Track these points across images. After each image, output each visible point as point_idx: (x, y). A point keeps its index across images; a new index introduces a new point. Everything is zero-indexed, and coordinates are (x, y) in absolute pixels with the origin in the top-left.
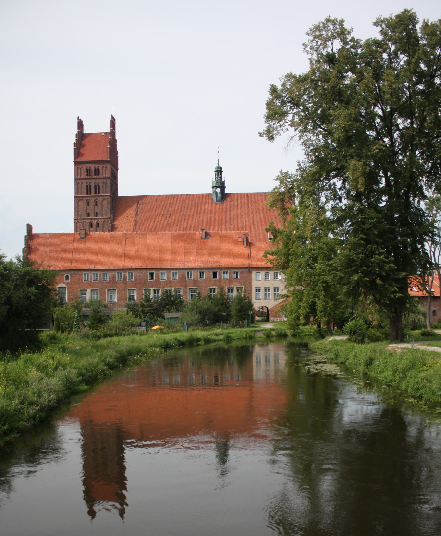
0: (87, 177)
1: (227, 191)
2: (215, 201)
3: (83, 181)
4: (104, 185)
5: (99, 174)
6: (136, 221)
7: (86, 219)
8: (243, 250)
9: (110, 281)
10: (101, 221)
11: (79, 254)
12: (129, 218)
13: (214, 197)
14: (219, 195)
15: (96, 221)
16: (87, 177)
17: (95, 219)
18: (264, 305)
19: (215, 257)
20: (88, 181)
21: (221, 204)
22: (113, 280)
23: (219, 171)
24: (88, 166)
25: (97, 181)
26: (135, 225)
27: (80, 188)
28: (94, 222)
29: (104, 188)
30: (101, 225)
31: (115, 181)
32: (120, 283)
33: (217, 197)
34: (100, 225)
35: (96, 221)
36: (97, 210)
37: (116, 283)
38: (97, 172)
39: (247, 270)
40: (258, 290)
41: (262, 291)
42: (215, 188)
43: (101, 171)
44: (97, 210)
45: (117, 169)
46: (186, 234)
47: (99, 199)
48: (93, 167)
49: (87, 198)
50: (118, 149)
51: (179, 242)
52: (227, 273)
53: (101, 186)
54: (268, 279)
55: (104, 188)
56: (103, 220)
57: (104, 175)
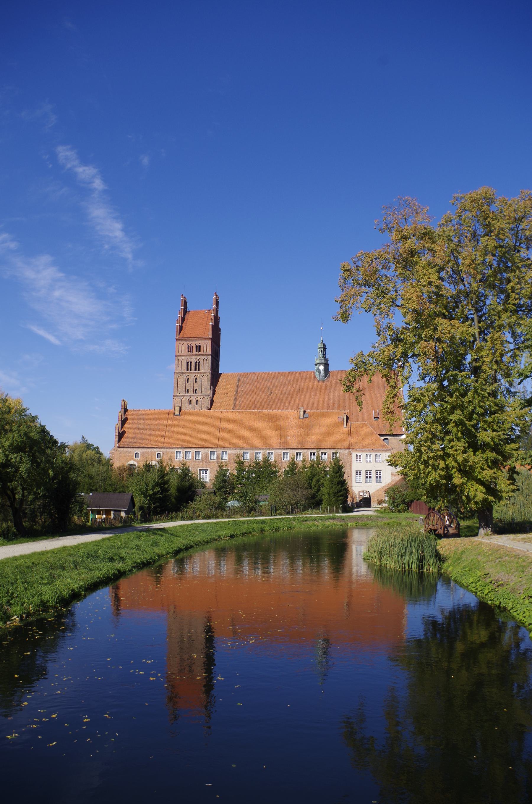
0: (188, 353)
1: (330, 368)
2: (318, 378)
3: (184, 357)
4: (205, 362)
5: (200, 351)
6: (236, 398)
7: (185, 396)
8: (342, 431)
9: (202, 460)
10: (199, 398)
11: (173, 432)
12: (228, 395)
13: (317, 374)
14: (322, 373)
15: (195, 397)
16: (188, 353)
17: (195, 396)
18: (366, 489)
19: (313, 437)
20: (189, 358)
21: (324, 382)
22: (206, 459)
23: (185, 303)
24: (190, 343)
25: (198, 358)
26: (235, 403)
27: (180, 365)
28: (193, 399)
29: (205, 365)
30: (199, 403)
31: (216, 358)
32: (213, 462)
33: (319, 375)
34: (192, 402)
35: (195, 397)
36: (197, 386)
37: (209, 463)
38: (198, 348)
39: (347, 451)
40: (358, 473)
41: (363, 473)
42: (318, 365)
43: (202, 348)
44: (197, 386)
45: (219, 346)
46: (283, 413)
47: (199, 376)
48: (194, 343)
49: (187, 375)
50: (221, 326)
51: (275, 421)
52: (325, 454)
53: (201, 363)
54: (360, 460)
55: (205, 365)
56: (202, 397)
57: (205, 352)
